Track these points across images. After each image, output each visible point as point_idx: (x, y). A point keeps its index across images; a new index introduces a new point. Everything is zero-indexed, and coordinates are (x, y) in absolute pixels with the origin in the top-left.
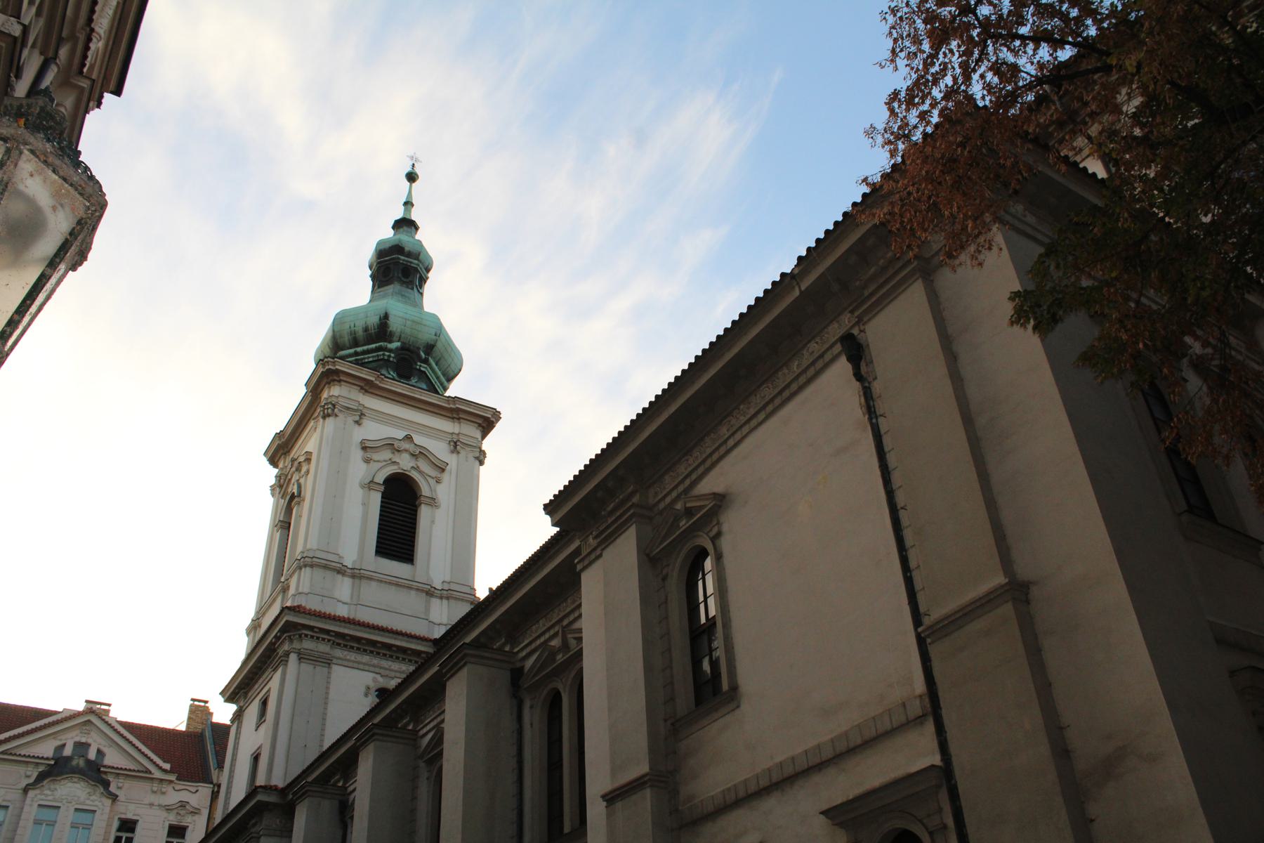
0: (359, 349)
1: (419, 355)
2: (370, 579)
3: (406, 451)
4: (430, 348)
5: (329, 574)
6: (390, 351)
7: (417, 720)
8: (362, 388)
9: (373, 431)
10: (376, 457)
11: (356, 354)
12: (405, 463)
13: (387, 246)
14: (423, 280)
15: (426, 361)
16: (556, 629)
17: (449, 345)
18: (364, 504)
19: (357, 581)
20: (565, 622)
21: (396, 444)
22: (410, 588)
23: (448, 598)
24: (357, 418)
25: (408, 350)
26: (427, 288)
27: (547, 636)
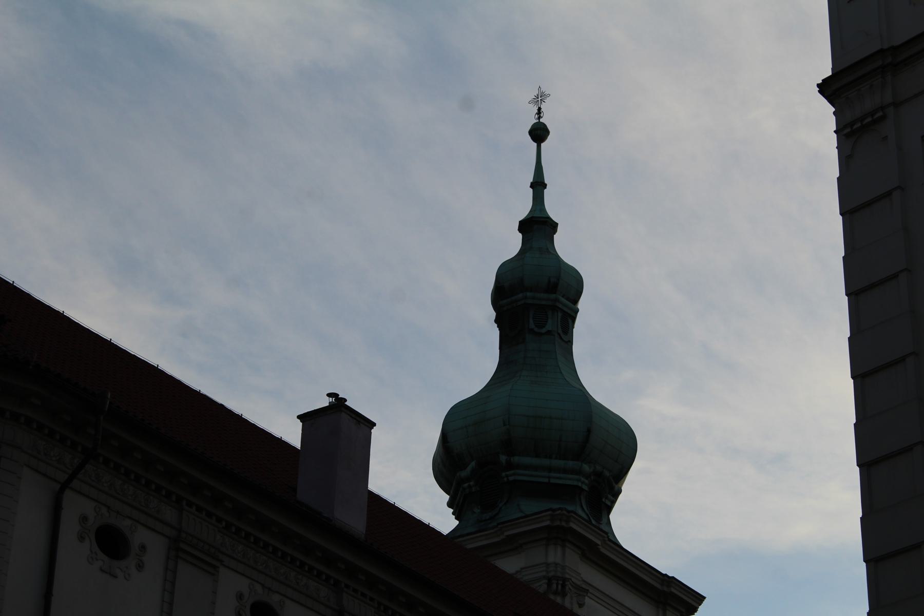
14: (570, 317)
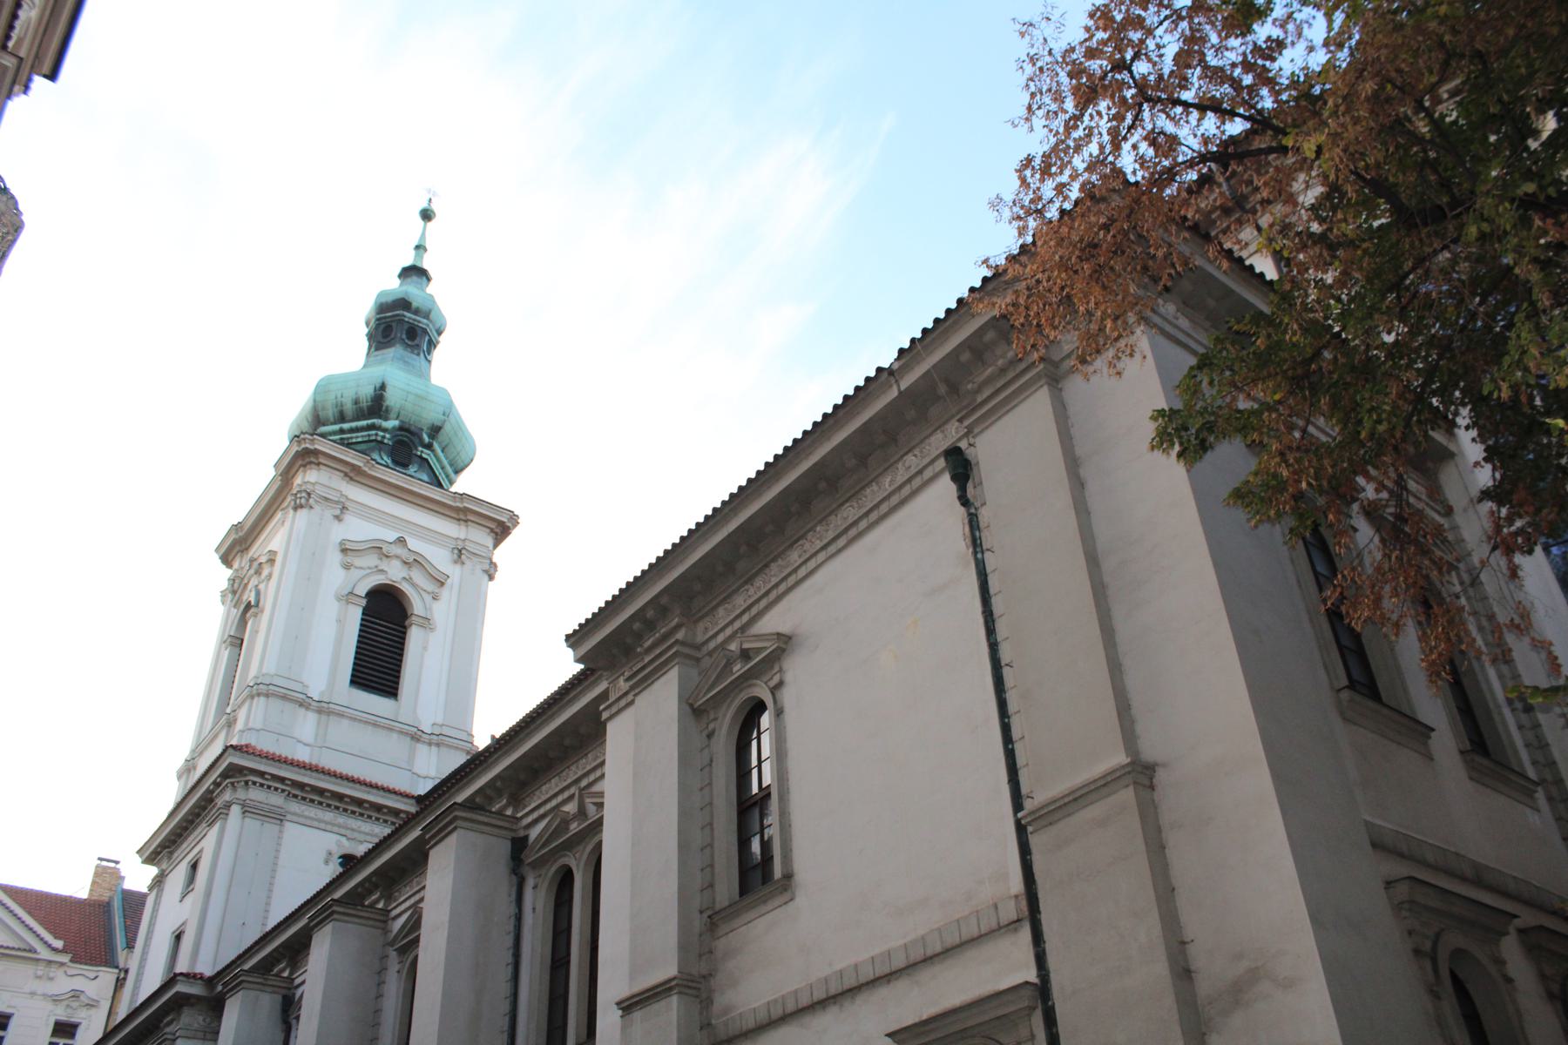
0: (346, 426)
1: (421, 439)
2: (341, 715)
3: (397, 557)
4: (435, 430)
5: (289, 706)
6: (385, 430)
7: (389, 897)
8: (346, 475)
9: (357, 529)
10: (358, 562)
11: (342, 431)
12: (394, 574)
13: (390, 299)
14: (432, 345)
15: (429, 446)
16: (572, 790)
17: (460, 428)
18: (339, 621)
19: (324, 717)
20: (584, 783)
21: (385, 548)
22: (391, 729)
23: (438, 745)
24: (338, 512)
25: (408, 430)
26: (438, 355)
27: (560, 798)
